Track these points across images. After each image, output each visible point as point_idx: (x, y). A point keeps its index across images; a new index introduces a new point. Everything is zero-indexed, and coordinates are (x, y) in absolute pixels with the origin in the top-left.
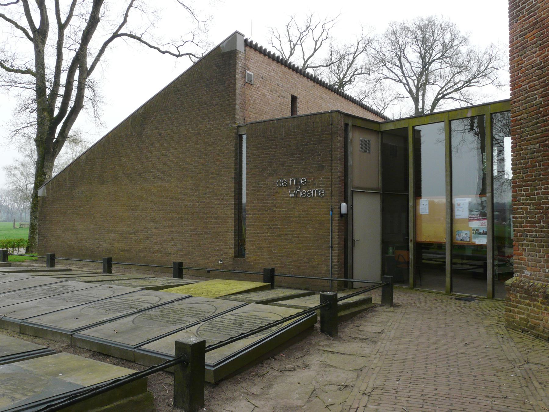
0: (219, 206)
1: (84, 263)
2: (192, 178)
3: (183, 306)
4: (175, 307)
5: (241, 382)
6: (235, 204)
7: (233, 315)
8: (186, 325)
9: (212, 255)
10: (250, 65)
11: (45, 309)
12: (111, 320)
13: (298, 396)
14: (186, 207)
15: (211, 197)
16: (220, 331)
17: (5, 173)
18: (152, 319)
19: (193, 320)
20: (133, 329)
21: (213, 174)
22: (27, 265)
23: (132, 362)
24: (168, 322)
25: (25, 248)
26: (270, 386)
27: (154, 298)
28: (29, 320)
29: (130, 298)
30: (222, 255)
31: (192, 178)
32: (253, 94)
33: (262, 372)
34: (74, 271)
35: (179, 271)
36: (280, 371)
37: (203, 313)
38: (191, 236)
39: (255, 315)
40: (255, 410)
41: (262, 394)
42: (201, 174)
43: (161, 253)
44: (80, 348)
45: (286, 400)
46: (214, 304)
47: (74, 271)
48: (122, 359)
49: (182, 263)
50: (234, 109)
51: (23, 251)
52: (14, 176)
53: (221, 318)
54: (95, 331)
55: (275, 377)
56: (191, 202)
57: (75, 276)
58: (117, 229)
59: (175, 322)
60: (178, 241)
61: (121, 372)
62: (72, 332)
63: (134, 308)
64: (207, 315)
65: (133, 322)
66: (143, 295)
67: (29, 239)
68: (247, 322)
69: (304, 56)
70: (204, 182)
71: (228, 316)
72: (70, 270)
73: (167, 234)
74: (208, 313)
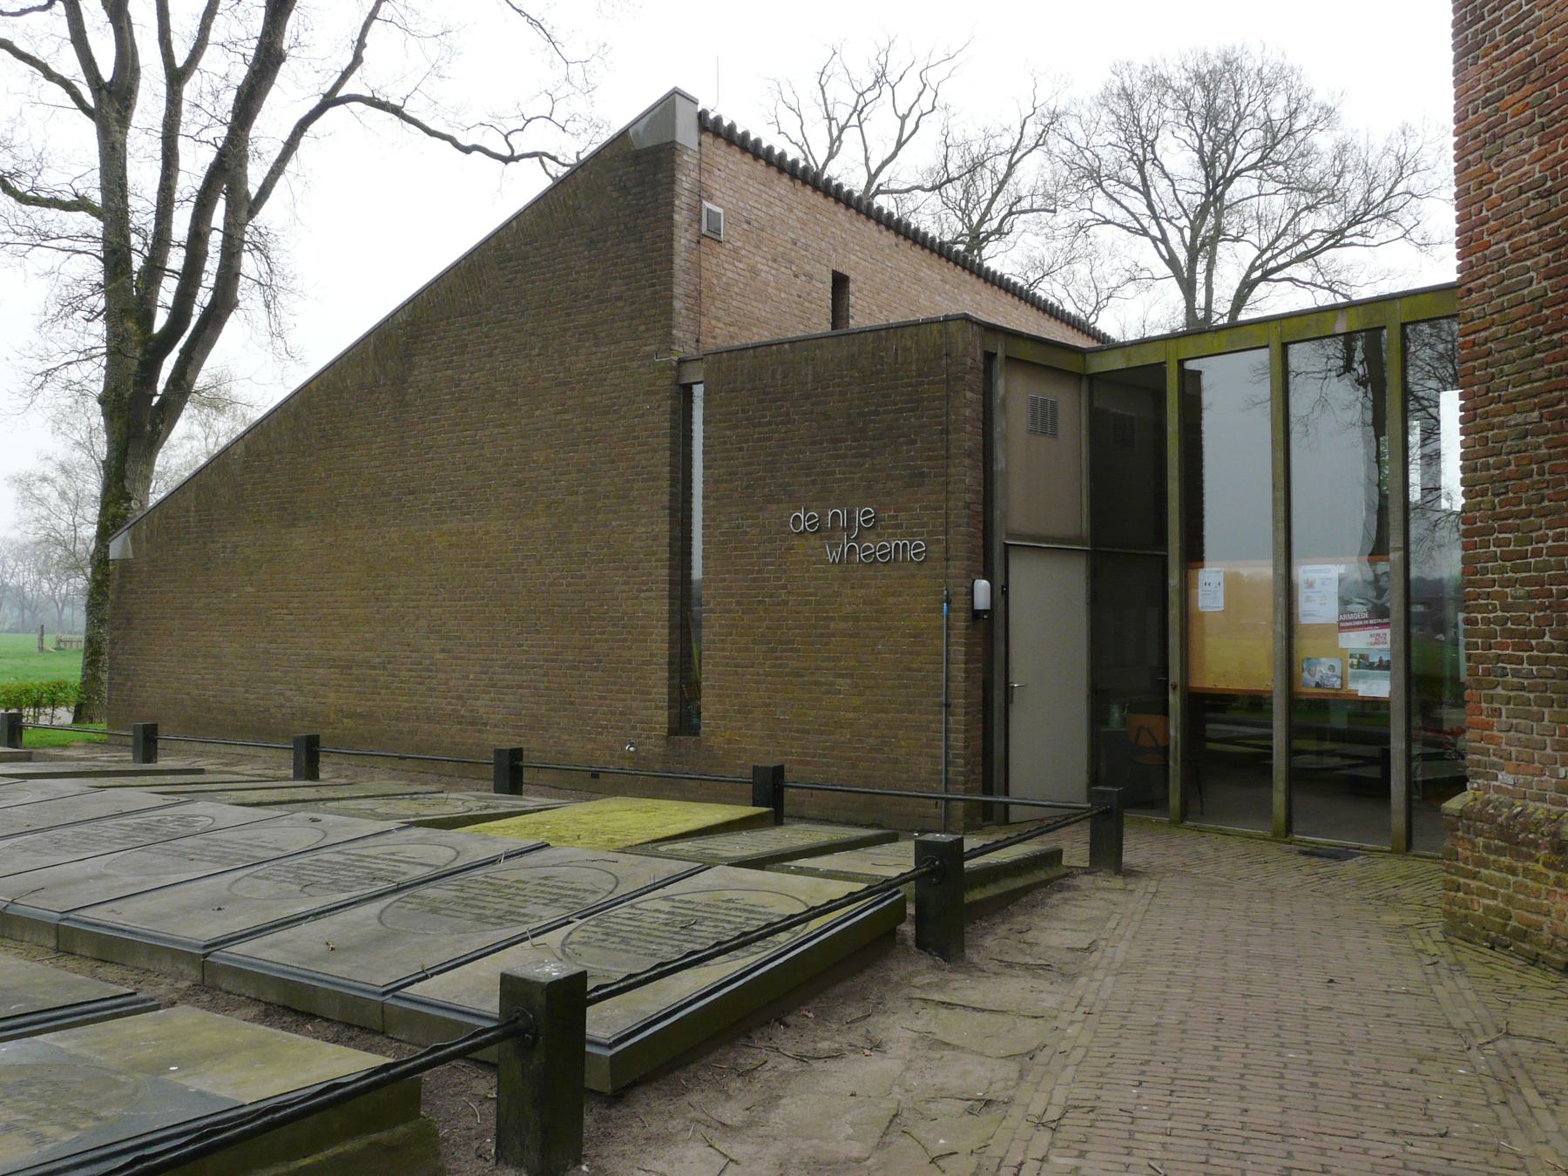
0: (626, 588)
1: (239, 750)
2: (548, 507)
3: (523, 875)
4: (499, 875)
5: (688, 1089)
6: (671, 583)
7: (666, 898)
8: (532, 926)
9: (606, 727)
10: (715, 184)
11: (129, 881)
12: (317, 915)
13: (850, 1131)
14: (530, 591)
15: (601, 561)
16: (628, 944)
17: (13, 493)
18: (434, 911)
19: (550, 914)
20: (381, 940)
21: (607, 497)
22: (78, 756)
23: (376, 1033)
24: (480, 918)
25: (72, 709)
26: (771, 1101)
27: (439, 849)
28: (81, 912)
29: (372, 852)
30: (634, 728)
31: (548, 507)
32: (723, 269)
33: (747, 1062)
34: (210, 772)
35: (510, 773)
36: (801, 1058)
37: (581, 895)
38: (546, 675)
39: (730, 900)
40: (728, 1170)
41: (749, 1124)
42: (574, 498)
43: (460, 723)
44: (228, 993)
45: (816, 1142)
46: (613, 868)
47: (210, 772)
48: (350, 1026)
49: (521, 750)
50: (669, 311)
51: (64, 715)
52: (41, 501)
53: (632, 906)
54: (272, 946)
55: (786, 1076)
56: (547, 576)
57: (214, 787)
58: (334, 654)
59: (501, 920)
60: (508, 687)
61: (346, 1062)
62: (206, 947)
63: (381, 879)
64: (591, 900)
65: (379, 919)
66: (408, 842)
67: (83, 683)
68: (705, 918)
69: (867, 159)
70: (582, 518)
71: (651, 902)
72: (201, 771)
73: (477, 669)
74: (594, 892)
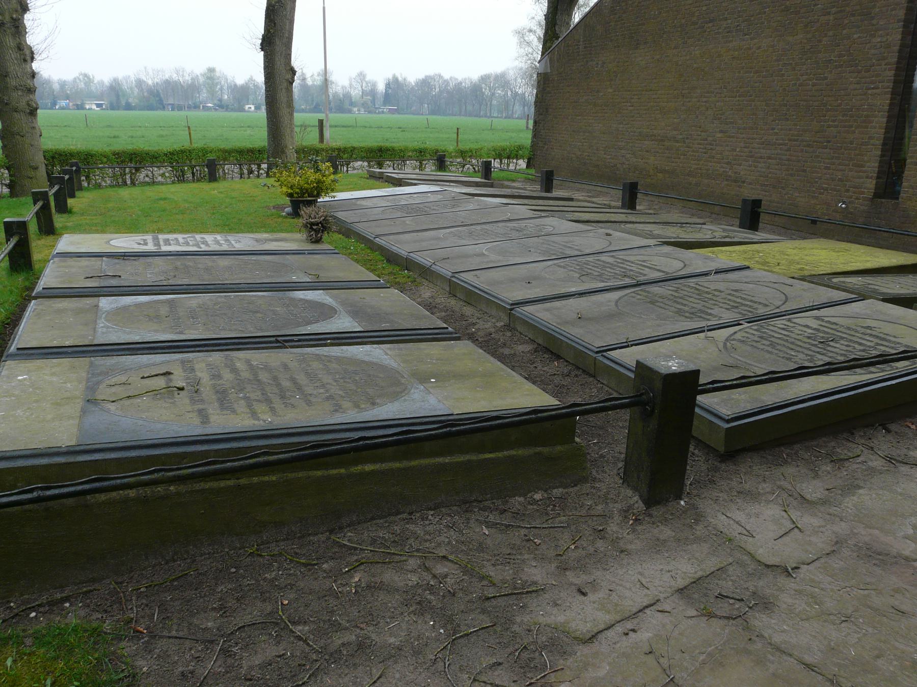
0: (858, 86)
1: (599, 189)
2: (806, 26)
3: (721, 286)
4: (705, 284)
5: (786, 462)
6: (895, 82)
7: (817, 318)
8: (710, 323)
9: (826, 189)
11: (494, 258)
12: (581, 294)
13: (911, 532)
14: (784, 90)
15: (841, 66)
16: (774, 347)
17: (515, 40)
18: (652, 302)
19: (728, 316)
20: (610, 316)
21: (853, 15)
22: (519, 187)
23: (591, 376)
24: (679, 312)
25: (526, 160)
26: (851, 488)
27: (672, 261)
28: (462, 274)
29: (632, 258)
30: (848, 191)
31: (806, 26)
33: (842, 452)
34: (578, 200)
35: (751, 216)
36: (890, 459)
37: (756, 306)
38: (789, 150)
39: (868, 327)
40: (792, 534)
41: (824, 502)
42: (827, 17)
43: (727, 180)
44: (521, 333)
45: (876, 532)
46: (787, 290)
47: (578, 200)
48: (578, 368)
49: (760, 201)
51: (522, 164)
52: (529, 44)
53: (789, 320)
54: (547, 310)
55: (872, 471)
56: (798, 79)
57: (566, 209)
58: (655, 132)
59: (693, 315)
60: (761, 158)
61: (522, 395)
62: (512, 304)
63: (629, 277)
64: (762, 311)
65: (616, 305)
66: (657, 255)
67: (532, 146)
68: (842, 338)
70: (831, 33)
71: (808, 320)
72: (571, 200)
73: (742, 145)
74: (766, 305)
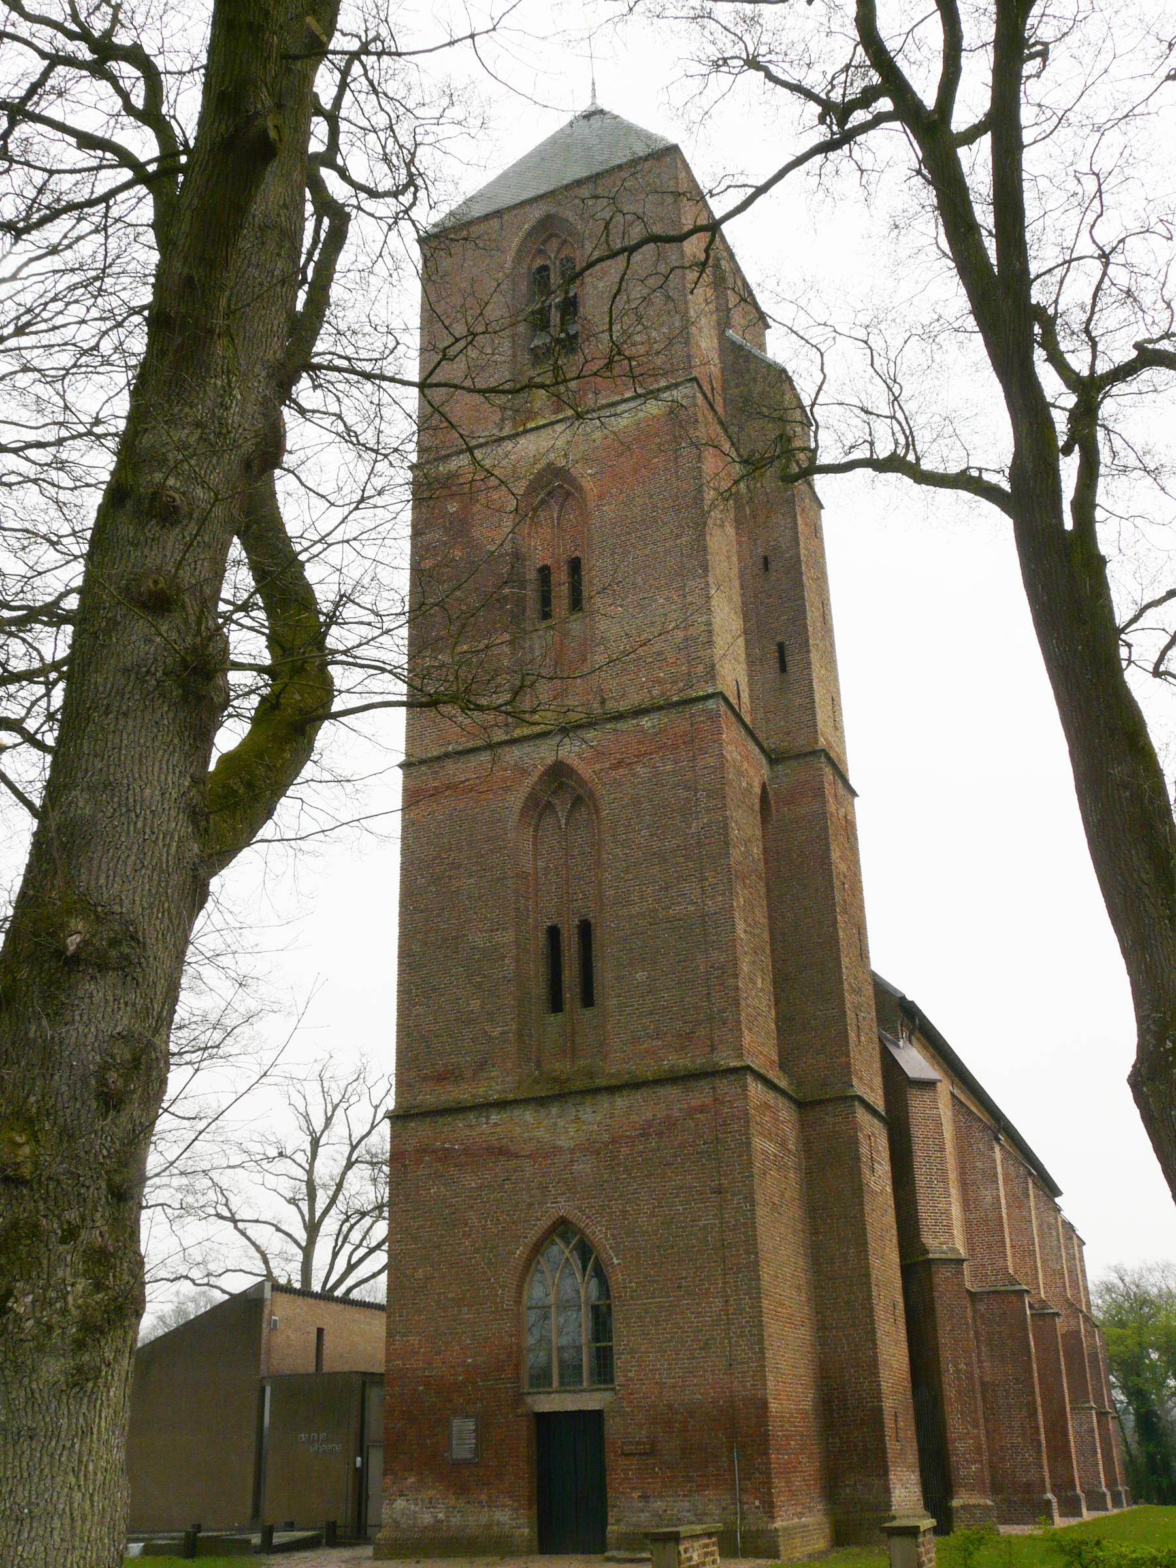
10: (276, 1309)
32: (279, 1339)
50: (259, 1359)
69: (350, 1136)
